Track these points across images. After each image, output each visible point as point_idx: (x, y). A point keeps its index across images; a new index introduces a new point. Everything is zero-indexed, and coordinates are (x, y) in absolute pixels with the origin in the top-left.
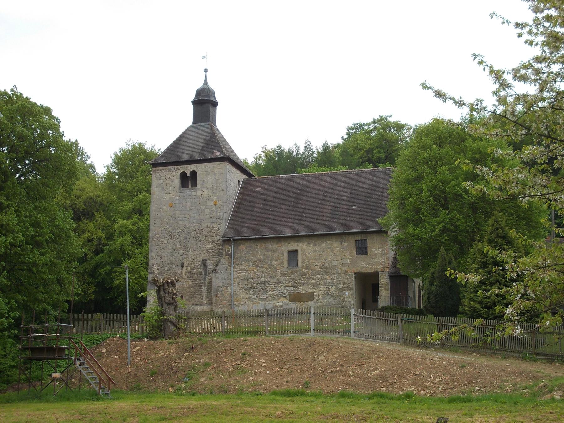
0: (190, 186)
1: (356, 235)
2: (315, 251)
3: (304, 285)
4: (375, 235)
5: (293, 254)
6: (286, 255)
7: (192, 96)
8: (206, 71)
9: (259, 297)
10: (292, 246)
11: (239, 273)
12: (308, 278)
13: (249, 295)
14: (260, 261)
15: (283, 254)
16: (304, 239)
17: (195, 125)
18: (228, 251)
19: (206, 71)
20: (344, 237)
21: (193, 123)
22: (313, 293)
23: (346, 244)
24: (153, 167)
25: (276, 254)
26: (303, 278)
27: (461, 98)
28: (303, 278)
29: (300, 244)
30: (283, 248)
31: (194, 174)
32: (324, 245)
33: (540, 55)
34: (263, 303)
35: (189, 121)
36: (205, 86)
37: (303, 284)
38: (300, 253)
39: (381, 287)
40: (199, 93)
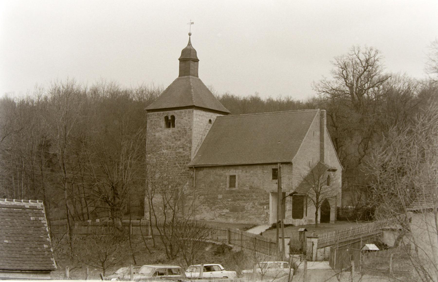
0: (171, 127)
1: (272, 165)
2: (247, 176)
3: (239, 200)
4: (247, 167)
5: (233, 177)
6: (228, 179)
7: (179, 55)
8: (190, 34)
9: (211, 208)
10: (232, 172)
11: (199, 191)
12: (241, 195)
13: (205, 207)
14: (212, 182)
15: (226, 178)
16: (240, 167)
17: (181, 77)
18: (192, 175)
19: (190, 34)
20: (265, 166)
21: (179, 76)
22: (244, 206)
23: (266, 171)
24: (148, 112)
25: (222, 178)
26: (238, 195)
27: (323, 76)
28: (238, 195)
29: (237, 171)
30: (227, 174)
31: (173, 117)
32: (252, 172)
33: (195, 110)
34: (214, 212)
35: (176, 74)
36: (189, 47)
37: (238, 200)
38: (237, 178)
39: (287, 203)
40: (184, 52)
